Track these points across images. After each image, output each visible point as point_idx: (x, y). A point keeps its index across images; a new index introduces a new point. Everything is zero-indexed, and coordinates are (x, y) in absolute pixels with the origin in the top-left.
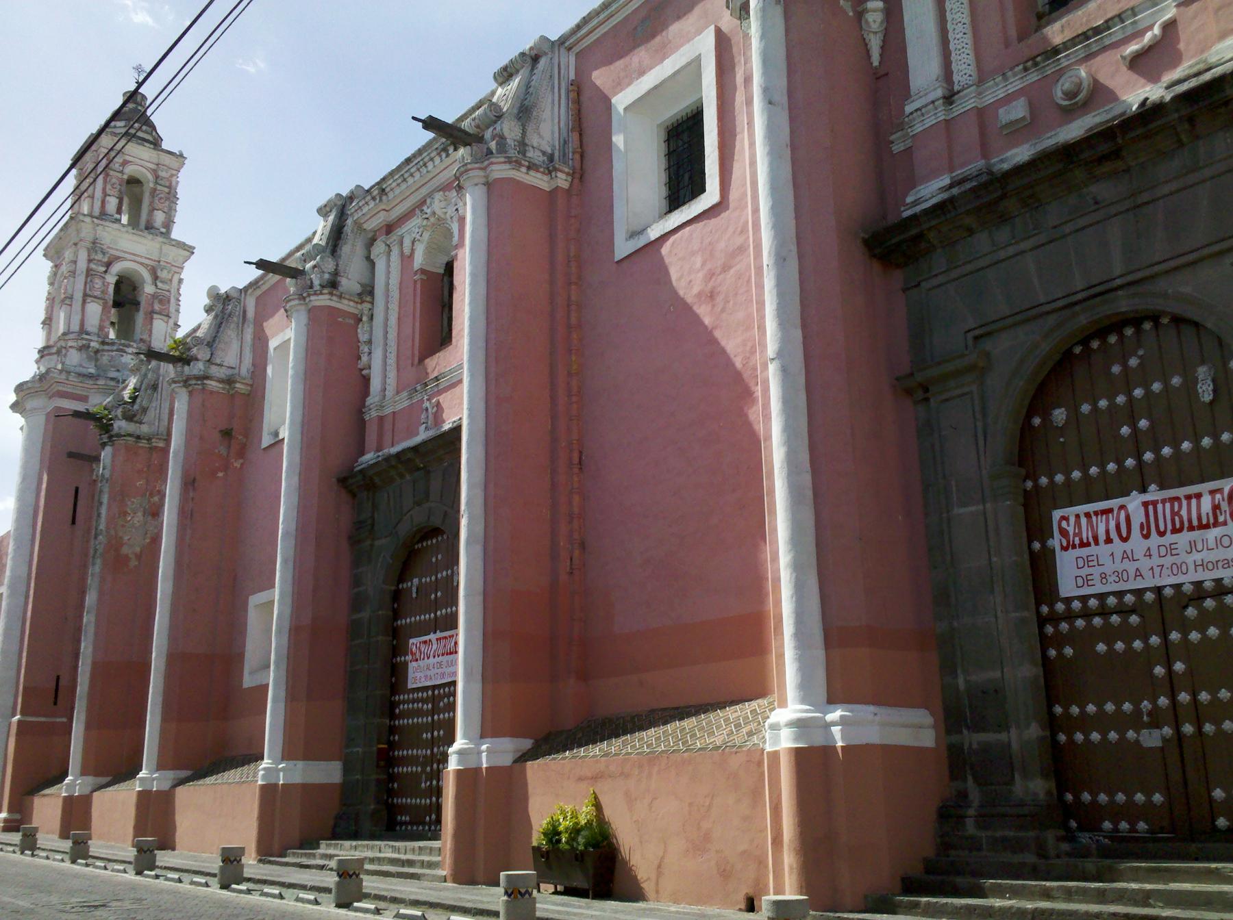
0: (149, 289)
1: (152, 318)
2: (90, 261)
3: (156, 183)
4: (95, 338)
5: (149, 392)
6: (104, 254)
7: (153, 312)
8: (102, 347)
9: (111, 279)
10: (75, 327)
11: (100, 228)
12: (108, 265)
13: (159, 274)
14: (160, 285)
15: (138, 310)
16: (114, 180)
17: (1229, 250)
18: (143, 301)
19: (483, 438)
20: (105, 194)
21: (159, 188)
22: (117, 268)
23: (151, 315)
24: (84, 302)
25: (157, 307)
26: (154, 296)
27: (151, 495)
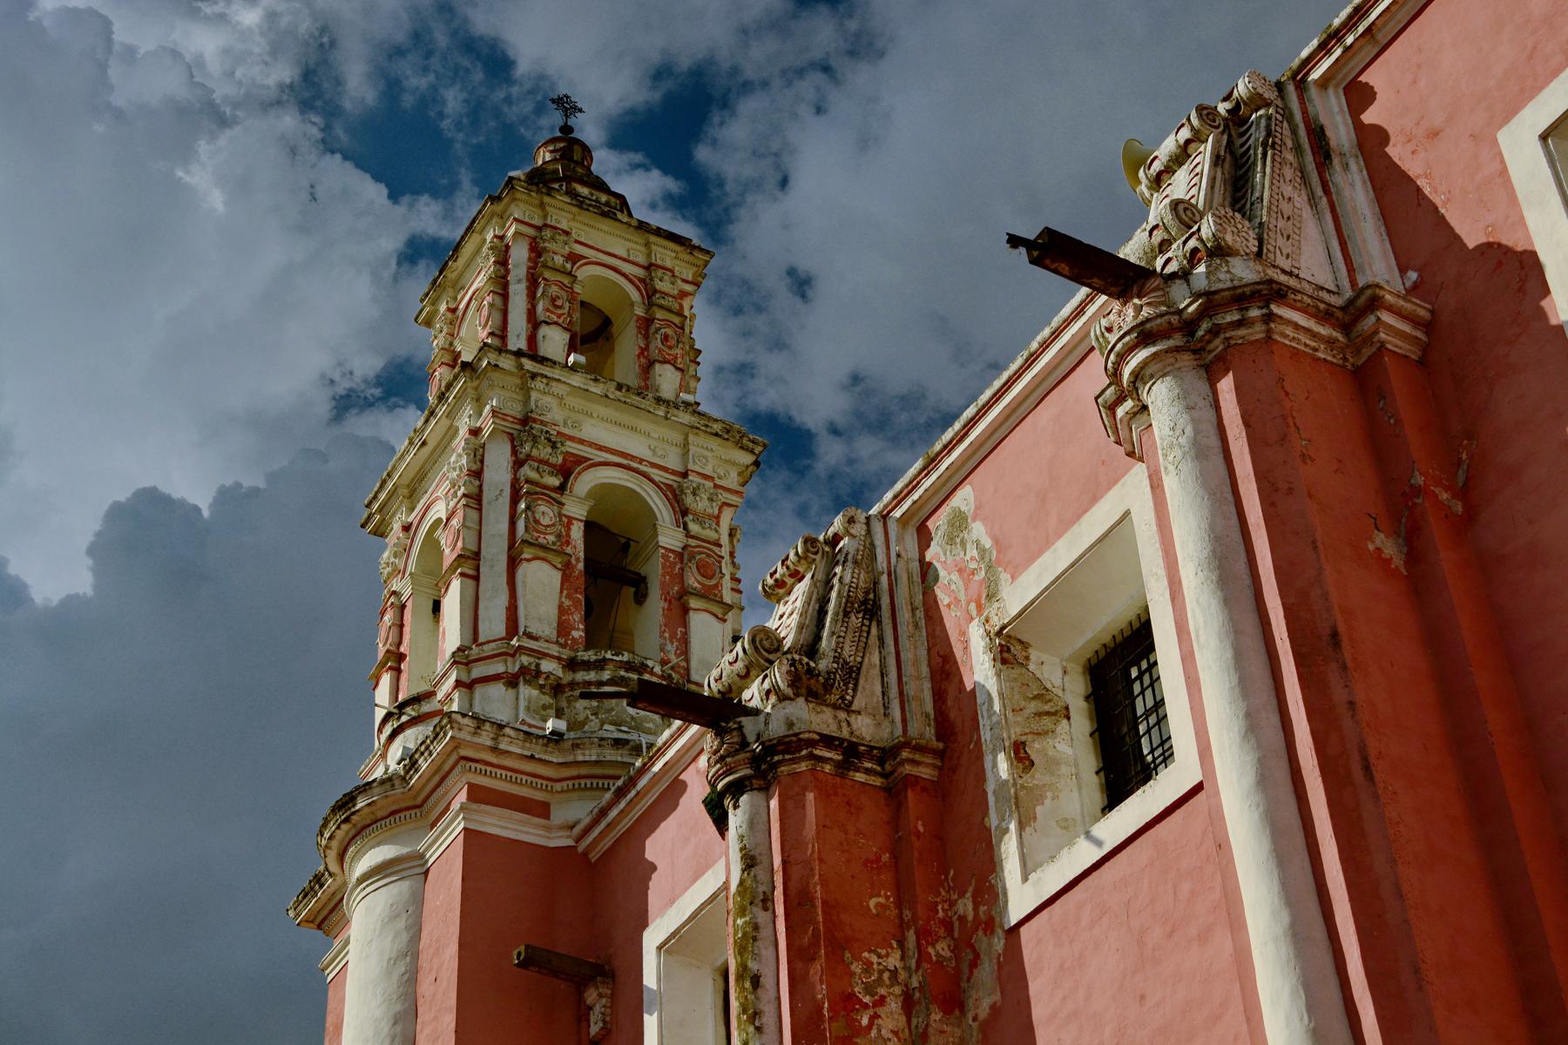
0: (670, 537)
1: (686, 610)
2: (518, 464)
3: (650, 305)
4: (554, 650)
5: (855, 620)
6: (554, 446)
7: (685, 592)
8: (567, 677)
9: (577, 509)
10: (493, 624)
11: (539, 384)
12: (567, 471)
13: (689, 500)
14: (694, 528)
15: (641, 598)
16: (554, 290)
17: (781, 1042)
18: (655, 571)
19: (1289, 782)
20: (534, 323)
21: (660, 314)
22: (586, 482)
23: (679, 611)
24: (513, 563)
25: (693, 580)
26: (683, 555)
27: (925, 936)
